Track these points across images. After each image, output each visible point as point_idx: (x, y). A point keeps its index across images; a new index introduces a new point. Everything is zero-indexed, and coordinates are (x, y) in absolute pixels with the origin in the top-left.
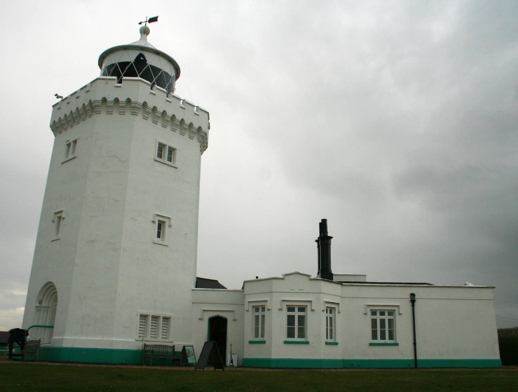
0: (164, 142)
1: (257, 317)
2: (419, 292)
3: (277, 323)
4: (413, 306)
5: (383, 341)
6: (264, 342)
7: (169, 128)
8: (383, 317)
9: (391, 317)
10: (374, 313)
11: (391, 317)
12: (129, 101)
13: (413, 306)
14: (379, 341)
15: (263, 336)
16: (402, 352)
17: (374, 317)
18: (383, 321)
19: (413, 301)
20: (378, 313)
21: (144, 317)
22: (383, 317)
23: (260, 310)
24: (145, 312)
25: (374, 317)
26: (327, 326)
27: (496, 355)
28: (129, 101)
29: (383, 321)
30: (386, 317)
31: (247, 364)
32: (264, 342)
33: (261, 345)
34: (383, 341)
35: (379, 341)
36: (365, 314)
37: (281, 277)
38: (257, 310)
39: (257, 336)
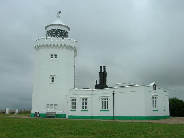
0: (52, 53)
1: (73, 102)
2: (116, 91)
3: (79, 105)
4: (114, 96)
5: (105, 109)
6: (75, 110)
7: (47, 49)
8: (105, 101)
9: (108, 101)
10: (83, 100)
11: (108, 101)
12: (65, 45)
13: (114, 96)
14: (85, 109)
15: (108, 108)
16: (110, 114)
17: (83, 101)
18: (105, 102)
19: (114, 94)
20: (85, 100)
21: (47, 105)
22: (105, 101)
23: (85, 100)
24: (48, 103)
25: (83, 101)
26: (155, 105)
27: (167, 113)
28: (65, 45)
29: (105, 102)
30: (106, 101)
31: (70, 117)
32: (75, 110)
33: (157, 111)
34: (105, 109)
35: (104, 109)
36: (99, 100)
37: (70, 90)
38: (73, 100)
39: (73, 108)
